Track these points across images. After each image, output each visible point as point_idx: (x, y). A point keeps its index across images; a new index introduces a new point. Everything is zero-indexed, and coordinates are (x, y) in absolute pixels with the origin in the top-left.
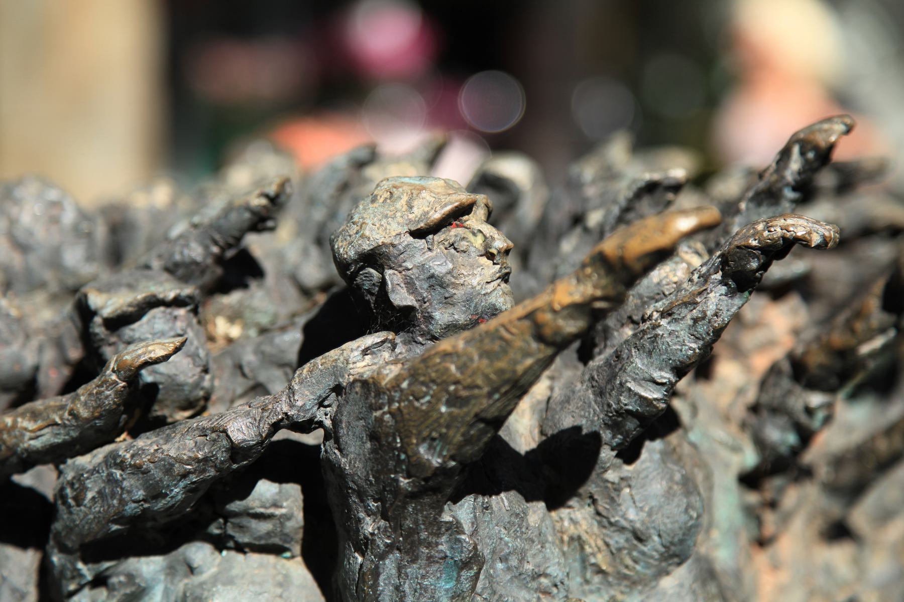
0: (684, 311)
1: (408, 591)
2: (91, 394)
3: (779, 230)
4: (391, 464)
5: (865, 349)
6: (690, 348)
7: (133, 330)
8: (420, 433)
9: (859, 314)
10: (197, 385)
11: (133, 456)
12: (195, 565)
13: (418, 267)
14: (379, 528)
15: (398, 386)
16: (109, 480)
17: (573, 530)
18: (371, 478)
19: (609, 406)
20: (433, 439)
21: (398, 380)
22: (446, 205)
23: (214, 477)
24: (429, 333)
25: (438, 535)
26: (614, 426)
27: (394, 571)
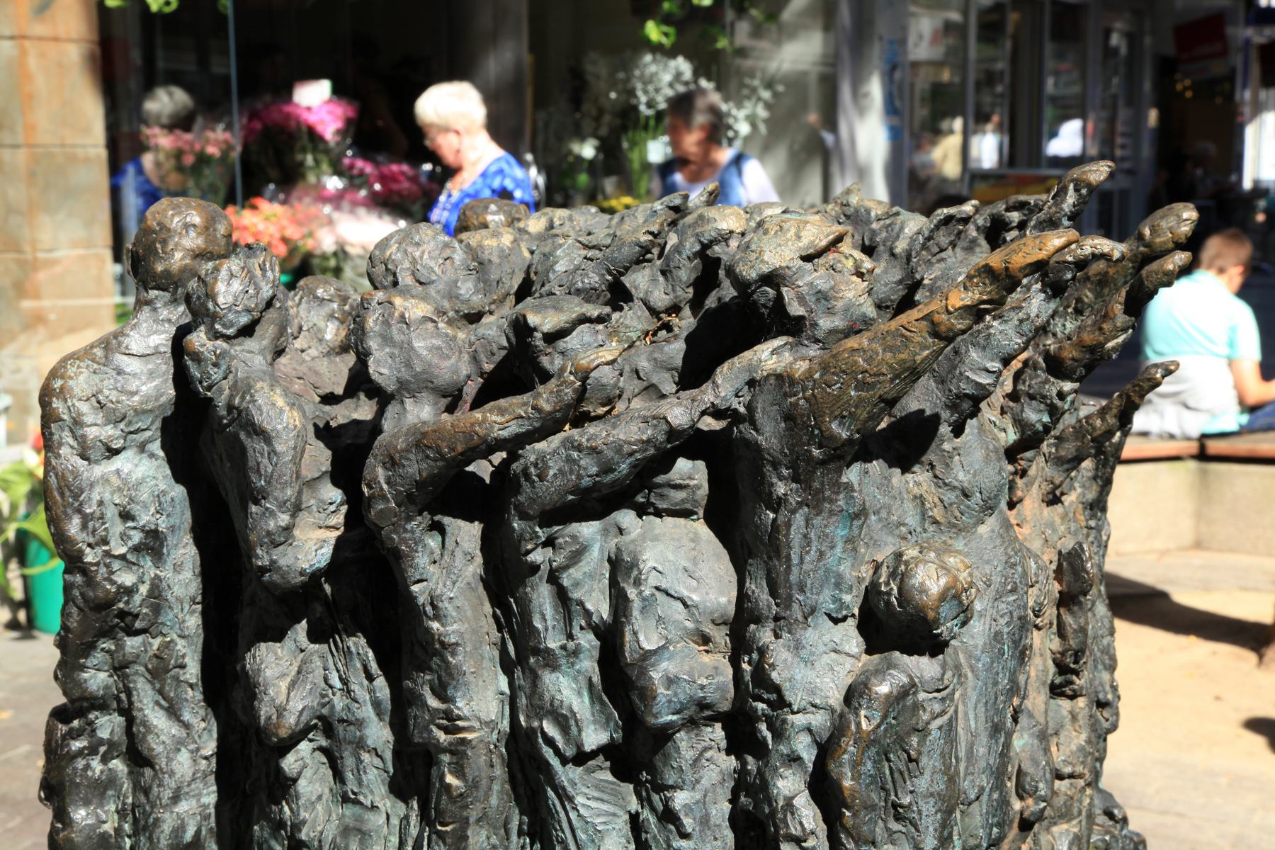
0: (1012, 314)
1: (813, 537)
2: (551, 392)
3: (1088, 247)
4: (805, 438)
5: (1110, 345)
6: (1016, 343)
7: (566, 342)
8: (832, 412)
9: (1106, 317)
10: (616, 386)
11: (588, 440)
12: (624, 526)
13: (807, 285)
14: (791, 490)
15: (811, 377)
16: (568, 460)
17: (916, 491)
18: (786, 450)
19: (950, 391)
20: (844, 417)
21: (809, 374)
22: (828, 235)
23: (653, 456)
24: (813, 337)
25: (838, 493)
26: (953, 407)
27: (803, 523)
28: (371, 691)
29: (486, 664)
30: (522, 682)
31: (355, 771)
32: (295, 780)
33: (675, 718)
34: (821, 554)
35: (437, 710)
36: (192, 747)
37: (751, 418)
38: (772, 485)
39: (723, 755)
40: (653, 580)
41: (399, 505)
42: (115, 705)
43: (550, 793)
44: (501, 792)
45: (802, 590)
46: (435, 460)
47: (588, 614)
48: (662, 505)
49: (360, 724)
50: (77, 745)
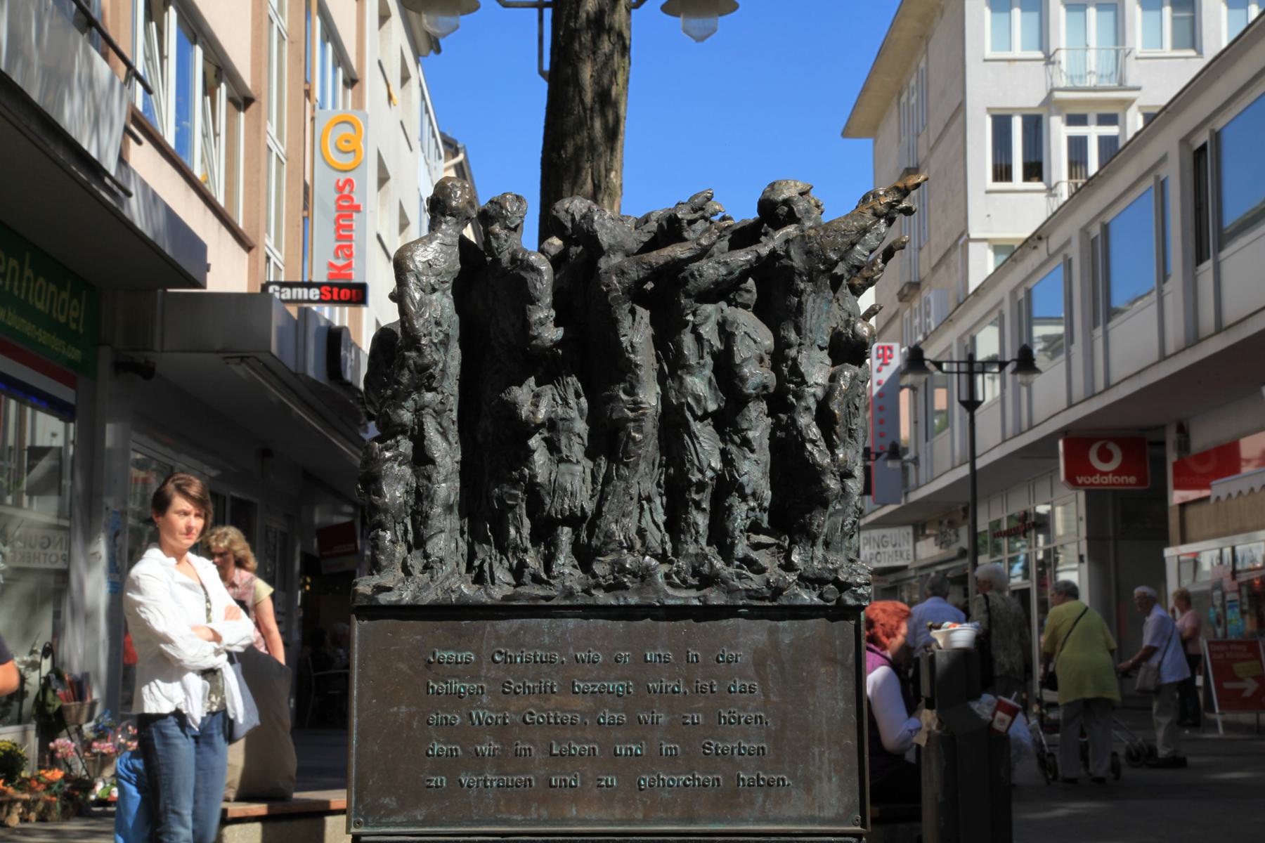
30: (672, 385)
31: (568, 446)
35: (628, 401)
37: (788, 256)
38: (798, 284)
40: (744, 329)
41: (623, 294)
43: (686, 437)
48: (739, 300)
49: (572, 420)
50: (388, 454)
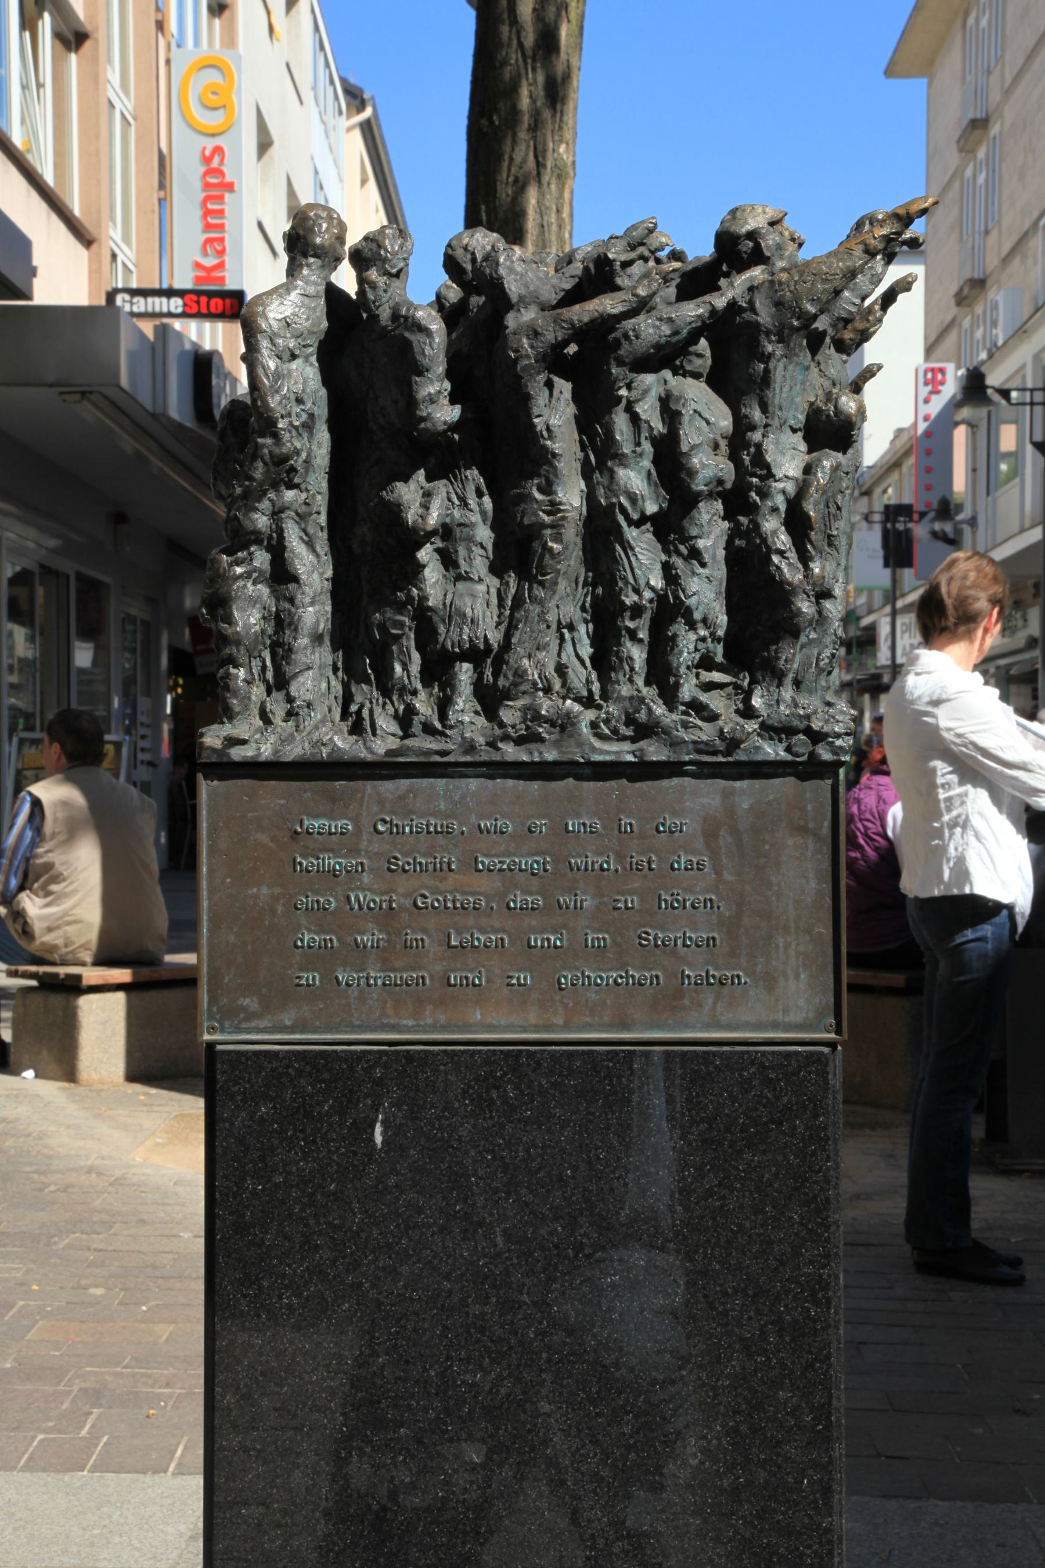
28: (480, 505)
29: (574, 472)
30: (600, 479)
32: (424, 566)
33: (705, 488)
34: (791, 388)
35: (543, 501)
36: (321, 570)
39: (720, 521)
40: (694, 406)
41: (536, 362)
42: (265, 543)
44: (577, 556)
45: (781, 409)
46: (567, 329)
47: (651, 428)
49: (472, 525)
50: (239, 570)
